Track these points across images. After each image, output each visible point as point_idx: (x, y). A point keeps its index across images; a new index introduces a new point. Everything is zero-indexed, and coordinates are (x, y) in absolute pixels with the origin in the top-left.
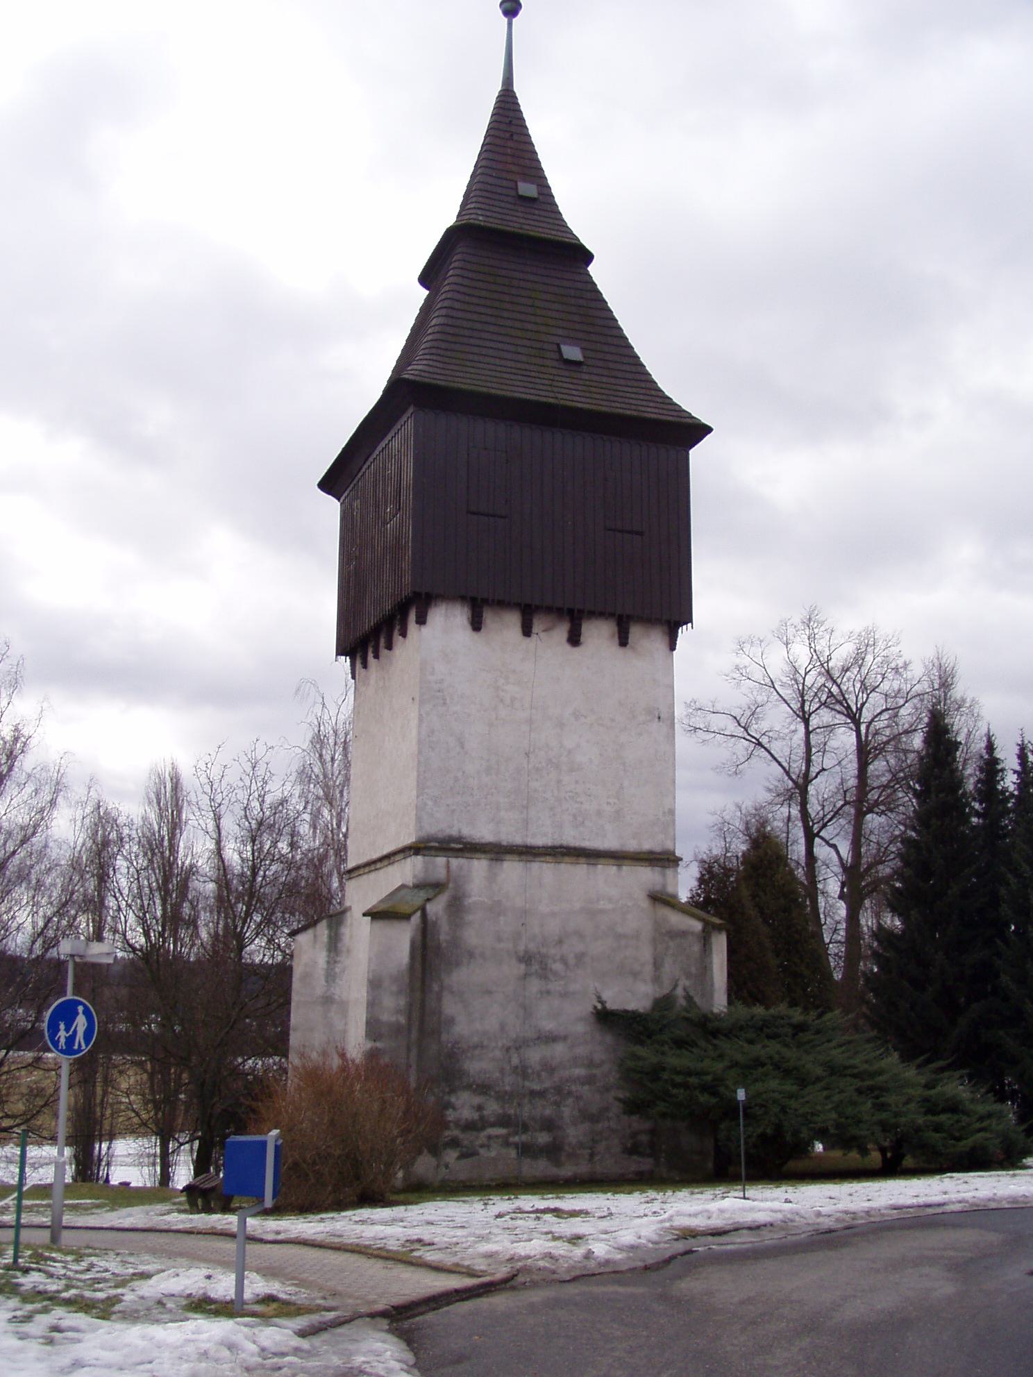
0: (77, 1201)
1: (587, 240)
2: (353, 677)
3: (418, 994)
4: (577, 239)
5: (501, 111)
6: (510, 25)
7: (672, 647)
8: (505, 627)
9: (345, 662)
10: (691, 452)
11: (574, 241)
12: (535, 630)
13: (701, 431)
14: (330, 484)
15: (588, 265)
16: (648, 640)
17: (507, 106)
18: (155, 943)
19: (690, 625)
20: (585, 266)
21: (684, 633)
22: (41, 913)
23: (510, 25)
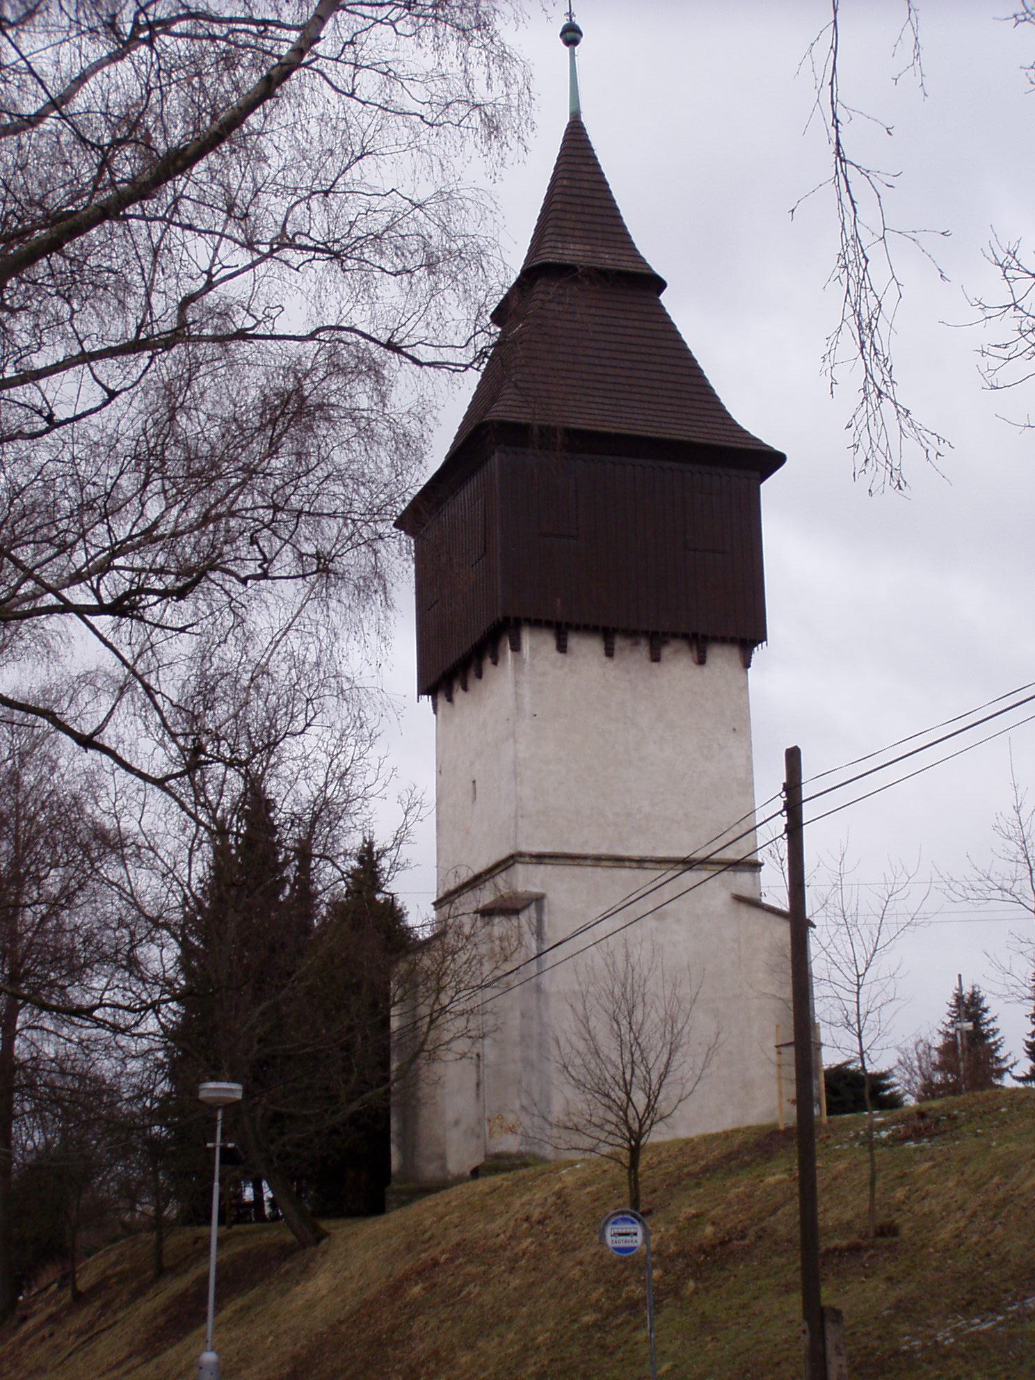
0: (216, 1184)
1: (659, 269)
2: (435, 712)
3: (646, 865)
4: (649, 268)
5: (571, 137)
6: (573, 55)
7: (747, 665)
8: (587, 649)
9: (426, 700)
10: (762, 486)
11: (646, 271)
12: (617, 652)
13: (771, 460)
14: (410, 521)
15: (659, 295)
16: (721, 659)
17: (576, 130)
18: (208, 677)
19: (764, 643)
20: (655, 295)
21: (758, 653)
22: (260, 1111)
23: (573, 55)
